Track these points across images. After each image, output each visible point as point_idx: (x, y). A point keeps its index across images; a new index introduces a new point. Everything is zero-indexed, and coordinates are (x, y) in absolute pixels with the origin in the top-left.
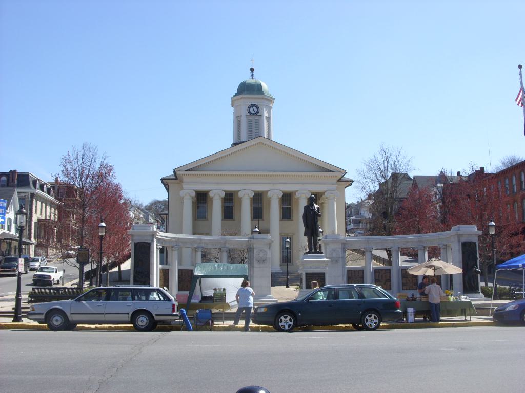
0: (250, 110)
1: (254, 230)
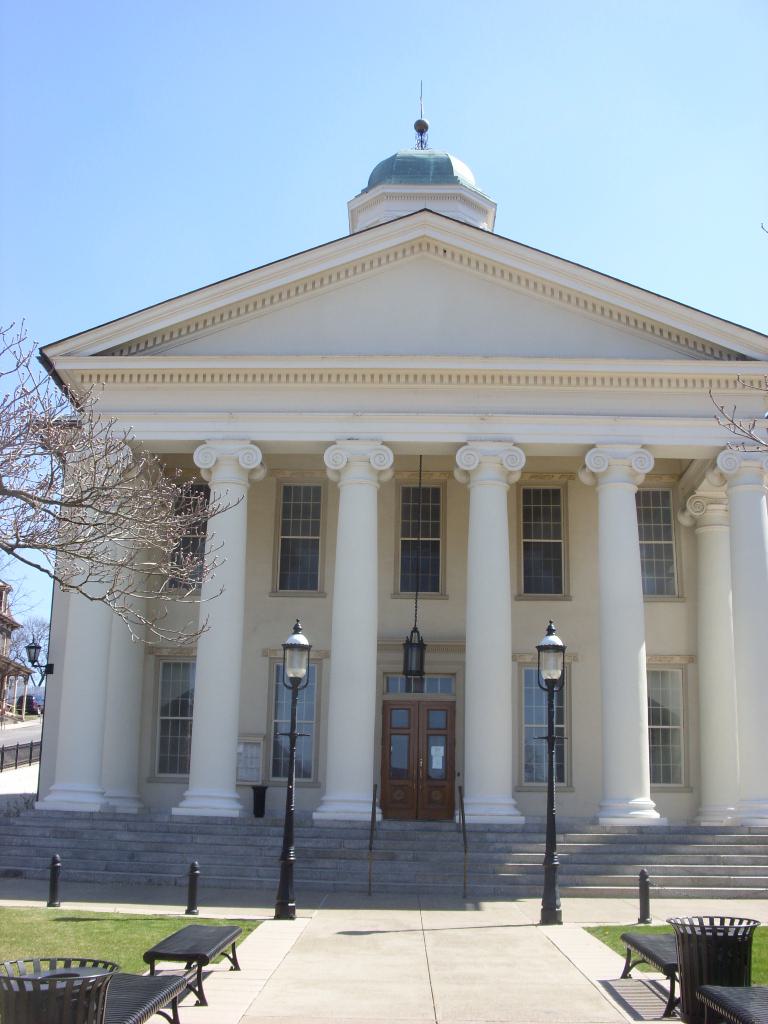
1: (289, 642)
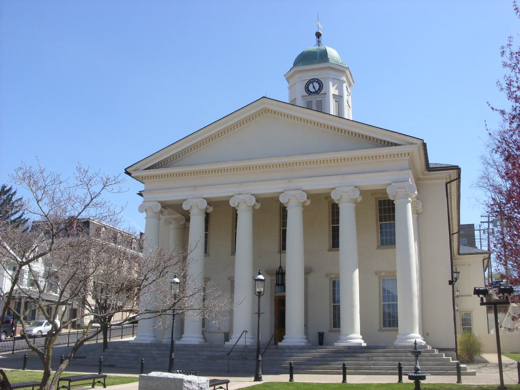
0: (308, 88)
1: (256, 278)
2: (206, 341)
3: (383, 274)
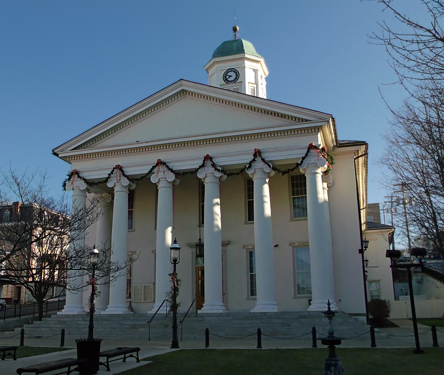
2: (227, 309)
3: (297, 244)
